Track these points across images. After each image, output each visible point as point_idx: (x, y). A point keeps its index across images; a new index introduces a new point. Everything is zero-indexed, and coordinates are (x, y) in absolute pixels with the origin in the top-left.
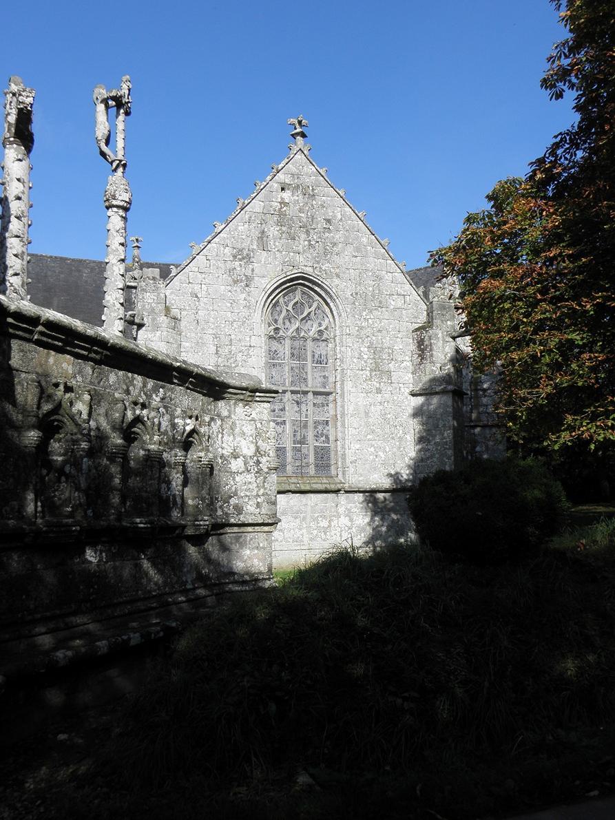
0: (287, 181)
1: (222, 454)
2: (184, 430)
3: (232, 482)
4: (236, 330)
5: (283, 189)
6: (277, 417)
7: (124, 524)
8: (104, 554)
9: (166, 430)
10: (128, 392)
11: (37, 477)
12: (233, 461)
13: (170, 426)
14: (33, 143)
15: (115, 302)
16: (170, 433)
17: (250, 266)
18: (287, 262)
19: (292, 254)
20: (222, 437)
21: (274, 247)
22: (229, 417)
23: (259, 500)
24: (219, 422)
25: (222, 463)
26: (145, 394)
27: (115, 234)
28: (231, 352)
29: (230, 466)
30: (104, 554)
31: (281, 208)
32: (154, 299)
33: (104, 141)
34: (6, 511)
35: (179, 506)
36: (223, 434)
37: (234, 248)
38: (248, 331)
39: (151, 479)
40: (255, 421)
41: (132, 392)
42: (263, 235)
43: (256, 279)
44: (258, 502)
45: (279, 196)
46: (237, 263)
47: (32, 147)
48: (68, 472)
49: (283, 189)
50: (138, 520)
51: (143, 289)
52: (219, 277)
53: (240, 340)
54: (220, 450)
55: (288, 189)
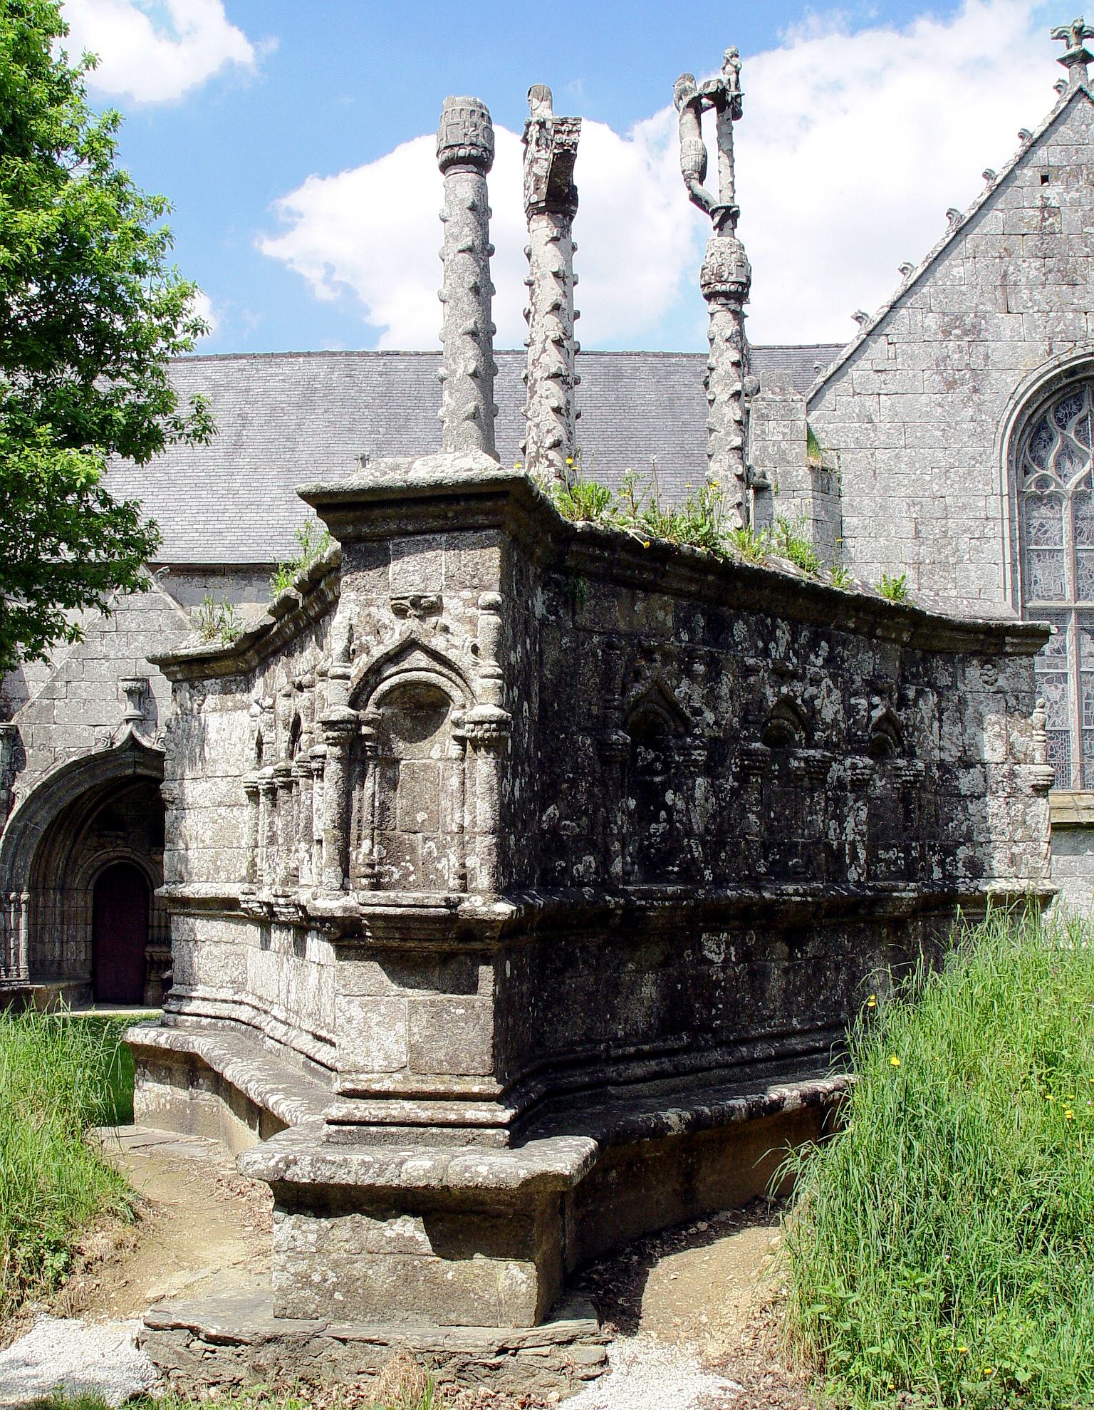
0: (1053, 161)
1: (941, 760)
2: (870, 718)
3: (961, 816)
4: (956, 486)
5: (1045, 179)
6: (1049, 666)
7: (766, 895)
8: (732, 949)
9: (835, 720)
10: (766, 653)
11: (623, 813)
12: (961, 773)
13: (842, 712)
14: (576, 206)
15: (728, 473)
16: (843, 726)
17: (981, 349)
18: (1060, 332)
19: (1071, 316)
20: (941, 727)
21: (1029, 304)
22: (954, 686)
23: (1016, 850)
24: (933, 699)
25: (940, 777)
26: (796, 654)
27: (724, 346)
28: (945, 532)
29: (956, 783)
30: (732, 949)
31: (1044, 220)
32: (784, 434)
33: (696, 175)
34: (577, 869)
35: (862, 862)
36: (940, 720)
37: (944, 314)
38: (980, 486)
39: (811, 814)
40: (1004, 693)
41: (773, 654)
42: (1005, 283)
43: (995, 374)
44: (1013, 854)
45: (1038, 196)
46: (951, 344)
47: (575, 212)
48: (670, 803)
49: (1045, 179)
50: (790, 888)
51: (762, 416)
52: (914, 376)
53: (964, 507)
54: (936, 752)
55: (1057, 179)
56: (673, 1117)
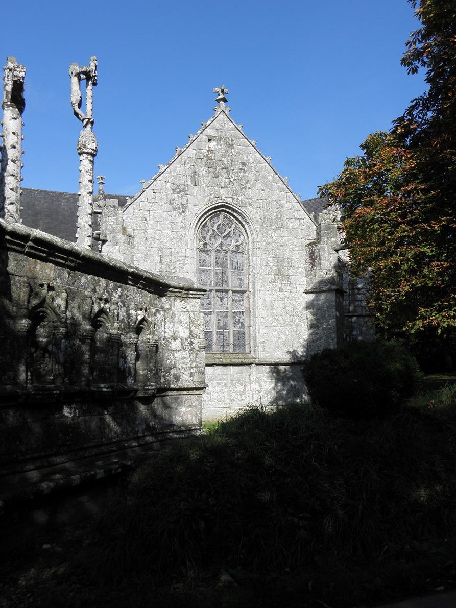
0: (213, 134)
1: (165, 337)
2: (137, 319)
3: (172, 358)
4: (175, 245)
5: (210, 140)
6: (206, 309)
7: (92, 388)
8: (77, 411)
9: (123, 319)
10: (95, 291)
11: (28, 354)
12: (172, 342)
13: (126, 316)
14: (24, 106)
15: (85, 224)
16: (126, 321)
17: (186, 197)
18: (213, 194)
19: (216, 188)
20: (165, 324)
21: (203, 183)
22: (170, 309)
23: (192, 371)
24: (162, 313)
25: (165, 343)
26: (108, 292)
27: (85, 173)
28: (171, 261)
29: (170, 345)
30: (77, 411)
31: (209, 154)
32: (114, 222)
33: (77, 104)
34: (4, 379)
35: (133, 375)
36: (165, 322)
37: (174, 184)
38: (184, 245)
39: (112, 355)
40: (189, 312)
41: (98, 291)
42: (195, 174)
43: (190, 207)
44: (191, 372)
45: (207, 146)
46: (175, 195)
47: (24, 109)
48: (50, 350)
49: (210, 140)
50: (102, 386)
51: (106, 214)
52: (162, 205)
53: (178, 252)
54: (163, 333)
55: (214, 140)
56: (433, 193)
